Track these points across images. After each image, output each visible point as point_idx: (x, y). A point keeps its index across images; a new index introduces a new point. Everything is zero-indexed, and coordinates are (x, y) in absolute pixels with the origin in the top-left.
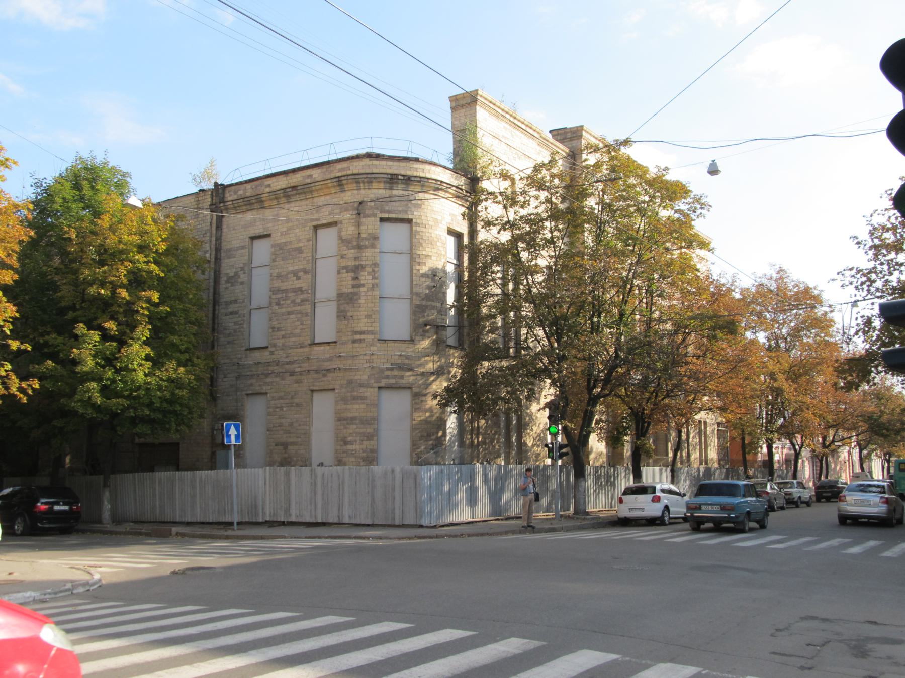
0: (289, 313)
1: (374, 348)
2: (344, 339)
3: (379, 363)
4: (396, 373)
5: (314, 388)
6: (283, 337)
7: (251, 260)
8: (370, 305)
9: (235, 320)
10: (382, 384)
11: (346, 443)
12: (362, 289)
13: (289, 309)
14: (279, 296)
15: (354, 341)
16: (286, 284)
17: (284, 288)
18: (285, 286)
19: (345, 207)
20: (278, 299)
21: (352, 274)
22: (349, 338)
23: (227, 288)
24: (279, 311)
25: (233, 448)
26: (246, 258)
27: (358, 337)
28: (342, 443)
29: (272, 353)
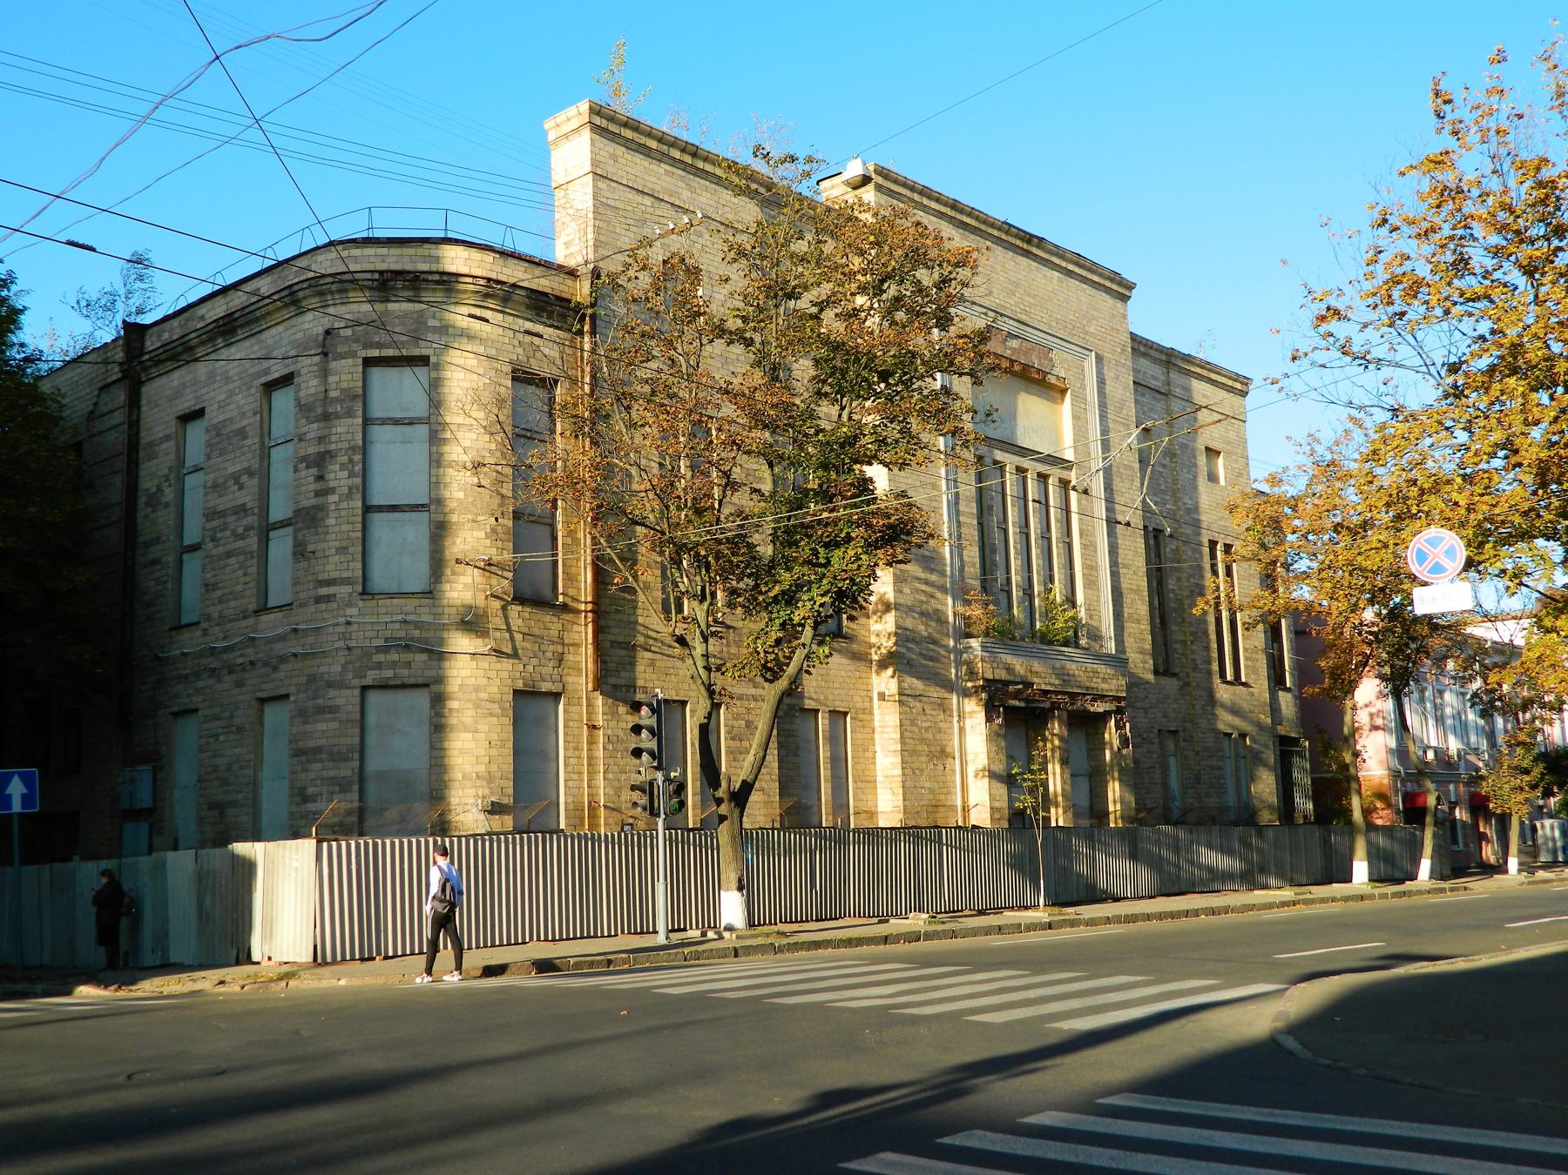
0: (229, 554)
1: (354, 611)
2: (302, 596)
3: (360, 639)
4: (394, 657)
5: (263, 695)
6: (220, 601)
7: (181, 461)
8: (345, 528)
9: (157, 575)
10: (368, 681)
11: (305, 799)
12: (333, 498)
13: (229, 547)
14: (215, 524)
15: (318, 600)
16: (224, 499)
17: (221, 508)
18: (224, 503)
19: (302, 349)
20: (214, 529)
21: (313, 471)
22: (312, 593)
23: (146, 517)
24: (215, 552)
25: (15, 820)
26: (172, 456)
27: (324, 591)
28: (298, 799)
29: (205, 632)
